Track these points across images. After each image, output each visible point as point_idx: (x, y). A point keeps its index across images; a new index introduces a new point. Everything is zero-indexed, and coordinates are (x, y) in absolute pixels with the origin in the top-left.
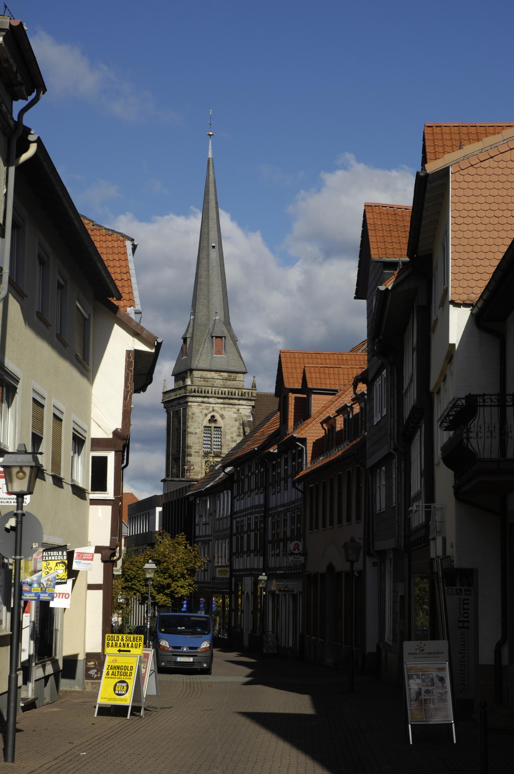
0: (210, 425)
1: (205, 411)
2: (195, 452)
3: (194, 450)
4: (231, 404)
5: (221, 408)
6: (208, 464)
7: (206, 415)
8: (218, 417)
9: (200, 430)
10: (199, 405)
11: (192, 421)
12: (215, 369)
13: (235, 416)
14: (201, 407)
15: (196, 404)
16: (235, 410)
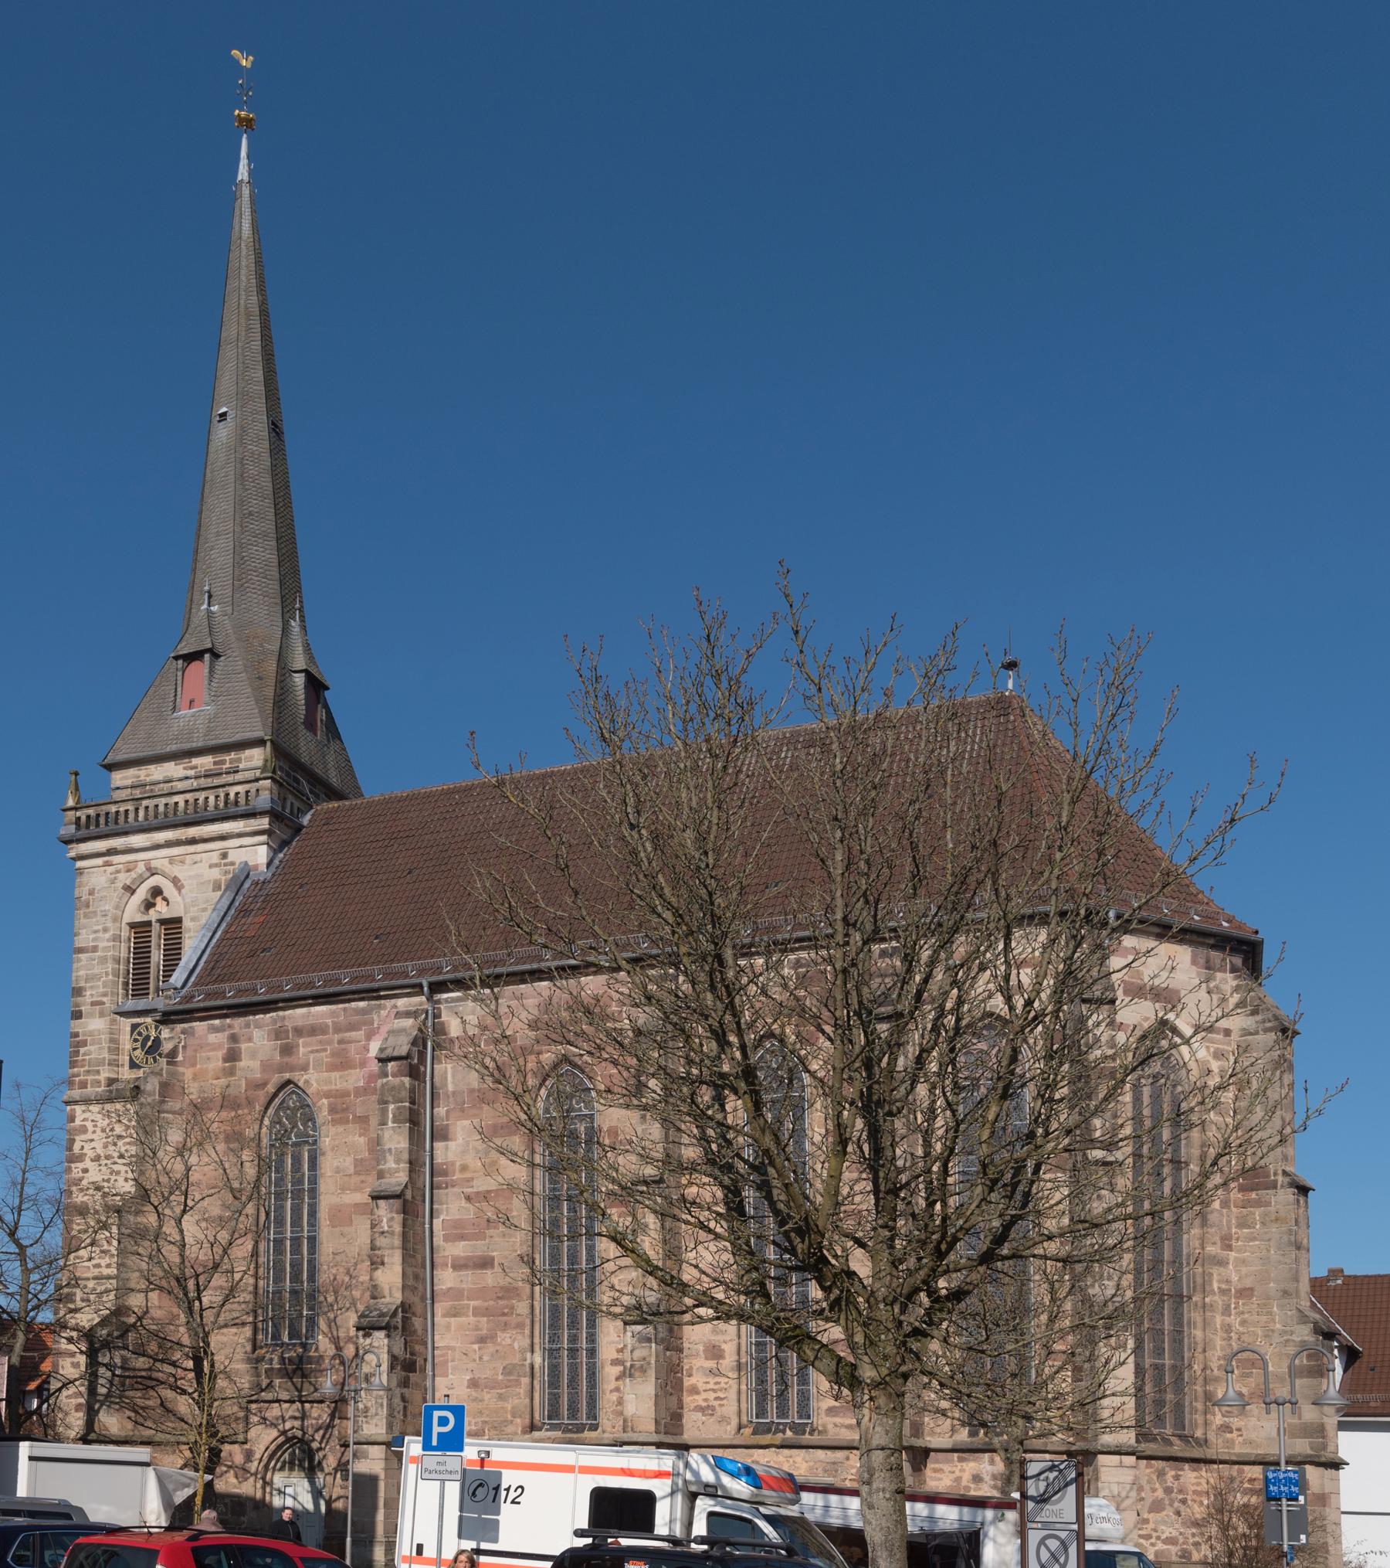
0: (145, 918)
1: (125, 879)
2: (93, 1004)
3: (89, 1000)
4: (193, 841)
5: (172, 860)
6: (140, 1034)
7: (131, 890)
8: (169, 889)
9: (980, 1188)
10: (108, 864)
11: (86, 916)
12: (174, 747)
13: (216, 874)
14: (110, 869)
15: (99, 861)
16: (215, 857)
